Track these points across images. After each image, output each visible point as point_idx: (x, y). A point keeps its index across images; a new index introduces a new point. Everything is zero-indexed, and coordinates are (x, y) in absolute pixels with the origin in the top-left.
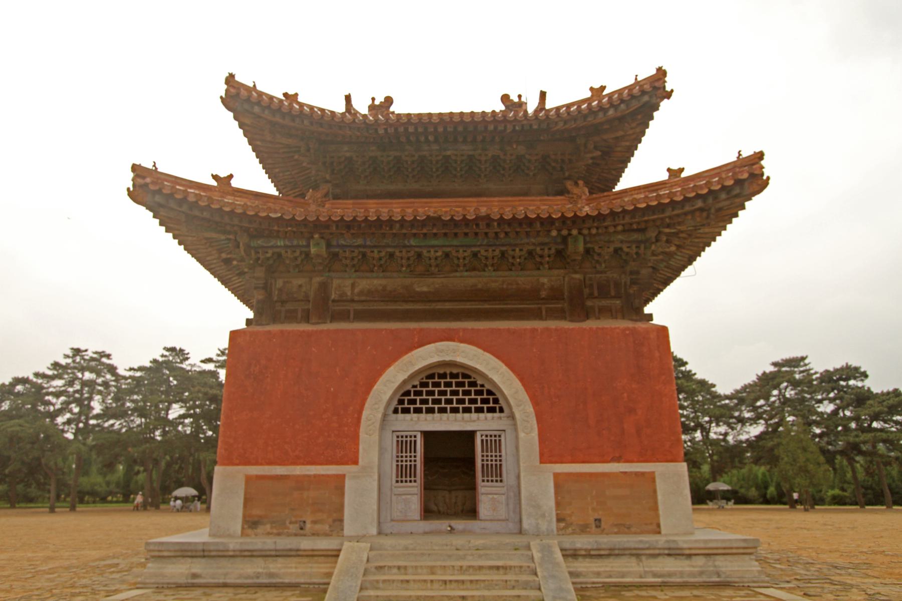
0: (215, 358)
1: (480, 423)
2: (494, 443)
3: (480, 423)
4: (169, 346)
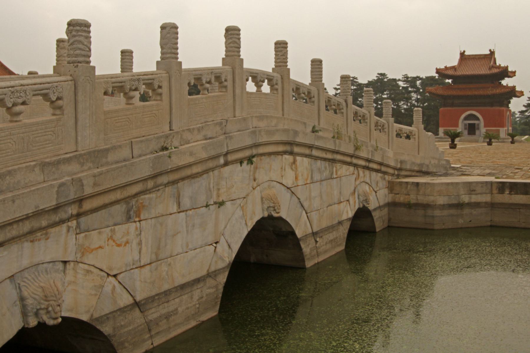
0: (401, 79)
1: (476, 122)
2: (478, 125)
3: (476, 122)
4: (380, 73)
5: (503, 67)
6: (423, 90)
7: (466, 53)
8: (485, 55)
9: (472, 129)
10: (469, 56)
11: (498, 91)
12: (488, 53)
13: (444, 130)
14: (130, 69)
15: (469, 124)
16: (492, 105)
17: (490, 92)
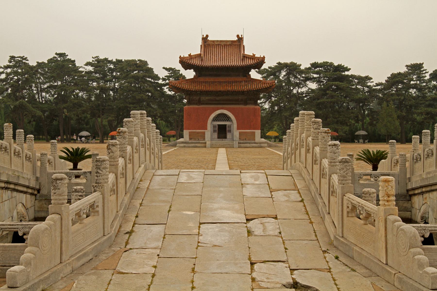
1: (227, 123)
2: (230, 126)
3: (227, 123)
5: (258, 58)
6: (115, 76)
8: (233, 41)
9: (222, 132)
10: (213, 41)
12: (236, 39)
13: (190, 132)
15: (218, 125)
16: (246, 103)
17: (235, 88)
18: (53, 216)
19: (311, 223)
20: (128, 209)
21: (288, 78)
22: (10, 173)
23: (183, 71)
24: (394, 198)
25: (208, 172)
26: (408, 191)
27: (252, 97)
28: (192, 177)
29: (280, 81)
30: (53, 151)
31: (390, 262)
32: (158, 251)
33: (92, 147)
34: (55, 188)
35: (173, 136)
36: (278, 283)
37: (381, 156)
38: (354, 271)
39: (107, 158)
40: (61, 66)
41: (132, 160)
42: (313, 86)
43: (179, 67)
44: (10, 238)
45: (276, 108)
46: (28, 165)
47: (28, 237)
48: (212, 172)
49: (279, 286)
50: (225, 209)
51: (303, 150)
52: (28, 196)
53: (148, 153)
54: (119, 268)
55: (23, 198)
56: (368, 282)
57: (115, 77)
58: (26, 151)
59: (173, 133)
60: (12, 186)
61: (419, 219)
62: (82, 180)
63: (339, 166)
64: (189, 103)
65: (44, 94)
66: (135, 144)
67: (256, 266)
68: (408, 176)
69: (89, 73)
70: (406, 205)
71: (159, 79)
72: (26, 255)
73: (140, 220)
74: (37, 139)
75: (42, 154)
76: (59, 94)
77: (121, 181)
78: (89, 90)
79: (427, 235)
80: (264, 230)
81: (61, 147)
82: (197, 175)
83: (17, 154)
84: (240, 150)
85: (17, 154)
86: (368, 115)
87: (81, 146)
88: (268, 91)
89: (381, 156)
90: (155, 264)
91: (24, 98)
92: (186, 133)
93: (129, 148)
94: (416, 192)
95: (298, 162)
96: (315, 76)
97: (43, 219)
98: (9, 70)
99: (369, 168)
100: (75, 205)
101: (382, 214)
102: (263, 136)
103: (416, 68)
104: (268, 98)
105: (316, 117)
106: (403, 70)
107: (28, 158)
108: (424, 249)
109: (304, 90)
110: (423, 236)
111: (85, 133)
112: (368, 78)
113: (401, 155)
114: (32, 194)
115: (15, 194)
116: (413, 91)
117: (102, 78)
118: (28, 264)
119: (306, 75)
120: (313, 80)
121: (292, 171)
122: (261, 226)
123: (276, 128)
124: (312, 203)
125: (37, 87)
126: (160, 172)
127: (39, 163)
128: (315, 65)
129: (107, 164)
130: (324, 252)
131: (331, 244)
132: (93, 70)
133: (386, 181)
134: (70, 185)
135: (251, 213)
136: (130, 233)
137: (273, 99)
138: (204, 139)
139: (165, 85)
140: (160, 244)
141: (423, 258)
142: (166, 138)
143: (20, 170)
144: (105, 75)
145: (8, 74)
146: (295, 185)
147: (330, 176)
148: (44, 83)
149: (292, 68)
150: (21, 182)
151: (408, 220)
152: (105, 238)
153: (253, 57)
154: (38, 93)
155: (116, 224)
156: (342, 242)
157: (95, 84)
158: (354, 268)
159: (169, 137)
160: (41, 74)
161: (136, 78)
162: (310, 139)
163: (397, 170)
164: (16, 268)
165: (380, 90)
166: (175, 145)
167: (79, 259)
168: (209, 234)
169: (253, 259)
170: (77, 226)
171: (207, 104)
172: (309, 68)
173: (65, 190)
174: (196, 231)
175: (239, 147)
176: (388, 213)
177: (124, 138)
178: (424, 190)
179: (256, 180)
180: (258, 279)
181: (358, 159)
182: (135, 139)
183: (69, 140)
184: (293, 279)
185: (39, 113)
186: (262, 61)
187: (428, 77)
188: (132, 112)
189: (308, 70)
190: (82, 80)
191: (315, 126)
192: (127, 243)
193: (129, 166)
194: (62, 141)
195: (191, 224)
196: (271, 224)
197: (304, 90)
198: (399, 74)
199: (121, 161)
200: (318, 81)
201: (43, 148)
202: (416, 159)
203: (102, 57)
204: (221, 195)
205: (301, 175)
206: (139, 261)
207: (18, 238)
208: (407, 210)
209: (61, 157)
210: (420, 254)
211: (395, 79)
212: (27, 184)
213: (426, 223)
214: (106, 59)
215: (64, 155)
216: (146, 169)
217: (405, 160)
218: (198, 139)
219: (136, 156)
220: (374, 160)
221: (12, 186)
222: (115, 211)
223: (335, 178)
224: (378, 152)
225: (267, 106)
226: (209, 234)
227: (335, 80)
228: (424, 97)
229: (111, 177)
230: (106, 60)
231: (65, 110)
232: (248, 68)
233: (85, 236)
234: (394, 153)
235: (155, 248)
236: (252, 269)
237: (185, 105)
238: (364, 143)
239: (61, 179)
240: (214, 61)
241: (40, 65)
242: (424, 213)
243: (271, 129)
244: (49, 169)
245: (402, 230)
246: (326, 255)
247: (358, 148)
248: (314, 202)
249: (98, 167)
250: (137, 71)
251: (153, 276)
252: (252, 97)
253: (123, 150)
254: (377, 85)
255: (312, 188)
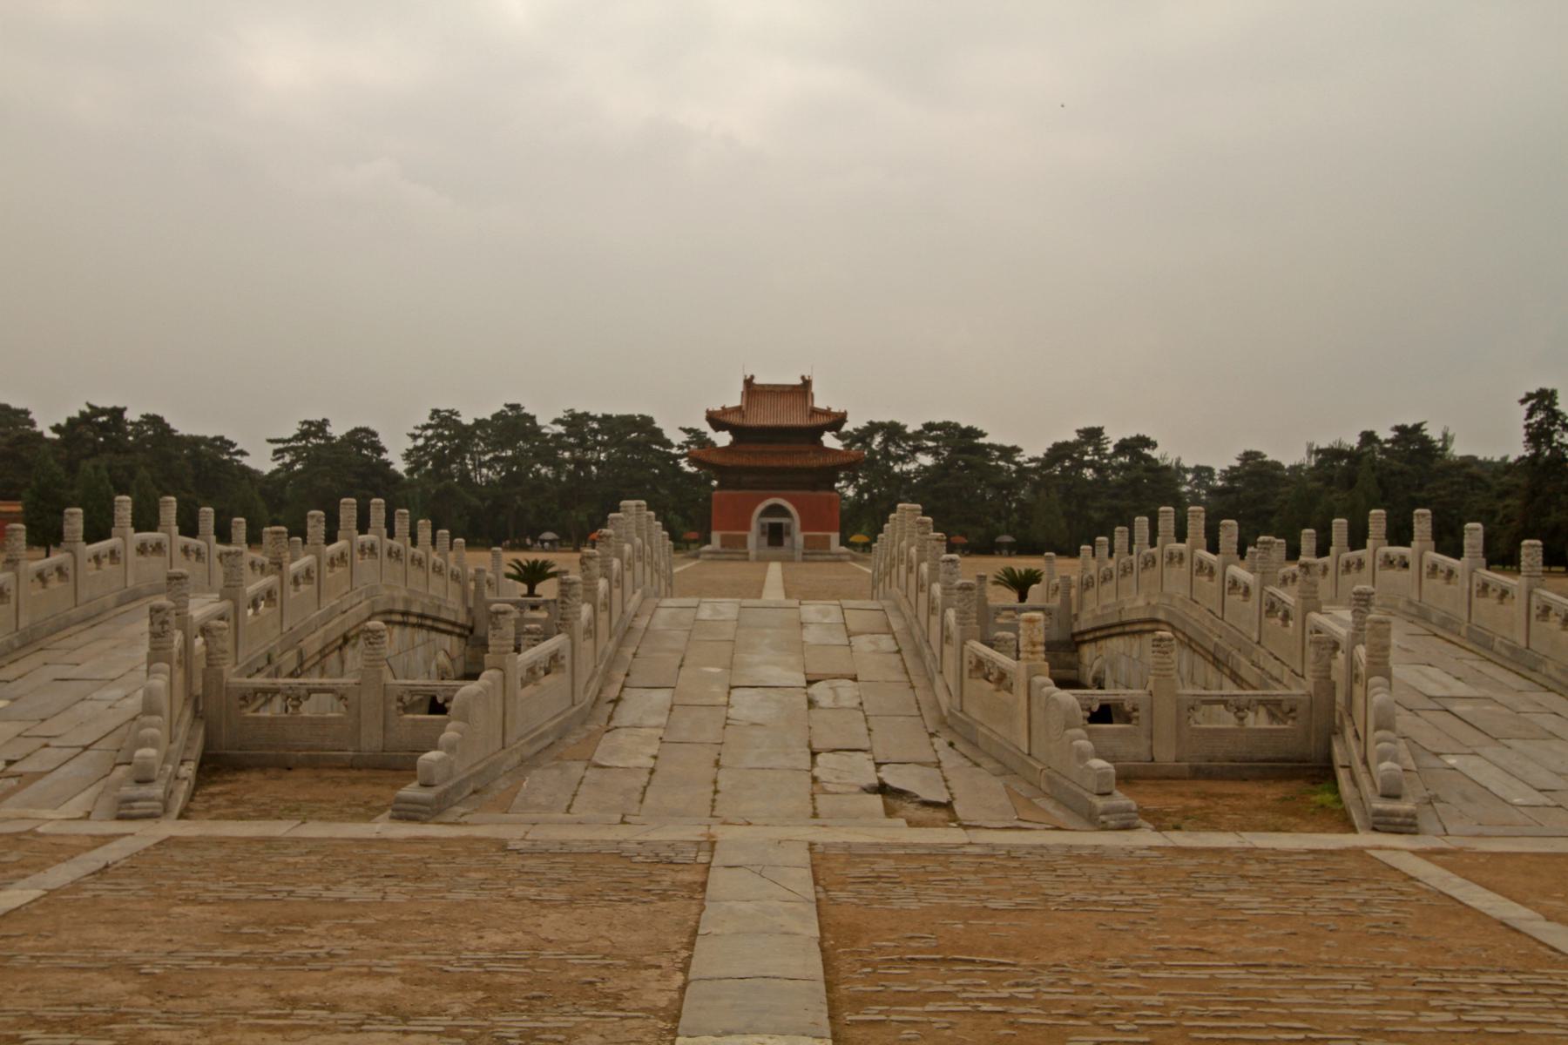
2: (788, 526)
5: (836, 414)
7: (757, 381)
9: (776, 535)
10: (763, 386)
11: (815, 462)
12: (800, 382)
14: (1411, 825)
15: (771, 525)
17: (798, 462)
18: (492, 672)
19: (913, 687)
20: (612, 662)
21: (886, 448)
22: (426, 601)
23: (712, 435)
24: (1042, 648)
25: (747, 602)
26: (1073, 635)
27: (824, 477)
28: (720, 610)
29: (873, 452)
30: (493, 565)
31: (1035, 752)
32: (660, 732)
33: (564, 560)
34: (496, 627)
35: (695, 541)
36: (853, 785)
37: (1032, 578)
38: (977, 765)
39: (578, 578)
40: (512, 425)
41: (620, 582)
42: (927, 460)
43: (705, 427)
44: (425, 706)
45: (866, 496)
46: (454, 587)
47: (452, 706)
48: (755, 602)
49: (856, 789)
50: (775, 664)
51: (903, 568)
52: (455, 639)
53: (648, 569)
54: (596, 759)
55: (448, 642)
56: (998, 783)
57: (600, 443)
58: (452, 565)
59: (693, 535)
60: (429, 622)
61: (1089, 681)
62: (542, 614)
63: (957, 595)
64: (720, 486)
65: (484, 471)
66: (626, 555)
67: (819, 758)
68: (1074, 611)
69: (558, 436)
70: (1070, 658)
71: (671, 445)
72: (450, 734)
73: (635, 679)
74: (471, 544)
75: (478, 571)
76: (509, 471)
77: (603, 616)
78: (558, 464)
79: (1095, 708)
80: (836, 698)
81: (509, 558)
82: (728, 608)
83: (438, 570)
84: (805, 565)
85: (438, 570)
86: (1016, 510)
87: (541, 557)
88: (851, 467)
89: (1032, 578)
90: (655, 752)
91: (453, 477)
92: (716, 537)
93: (616, 563)
94: (1087, 637)
95: (895, 588)
96: (930, 444)
97: (474, 676)
98: (430, 432)
99: (1012, 597)
100: (528, 655)
101: (1023, 674)
102: (844, 542)
103: (1093, 435)
104: (852, 479)
105: (924, 514)
106: (1072, 437)
107: (455, 577)
108: (1089, 732)
109: (912, 466)
110: (1089, 710)
111: (549, 535)
112: (1015, 450)
113: (1063, 578)
114: (460, 636)
115: (433, 635)
116: (1088, 473)
117: (579, 445)
118: (451, 748)
119: (917, 441)
120: (926, 450)
121: (886, 603)
122: (830, 693)
123: (865, 528)
124: (914, 655)
125: (472, 459)
126: (668, 602)
127: (472, 586)
128: (929, 427)
129: (579, 589)
130: (932, 735)
131: (943, 721)
132: (400, 467)
133: (1031, 621)
134: (520, 622)
135: (815, 669)
136: (616, 701)
137: (861, 481)
138: (745, 546)
139: (681, 456)
140: (663, 720)
141: (1086, 744)
142: (680, 543)
143: (442, 596)
144: (583, 440)
145: (428, 439)
146: (888, 625)
147: (944, 611)
148: (485, 453)
149: (893, 431)
150: (444, 615)
151: (1062, 684)
152: (575, 709)
153: (827, 413)
154: (474, 469)
155: (594, 687)
156: (961, 720)
157: (567, 454)
158: (979, 761)
159: (688, 542)
160: (481, 439)
161: (635, 445)
162: (913, 550)
163: (1056, 602)
164: (433, 755)
165: (1035, 470)
166: (696, 557)
167: (532, 742)
168: (745, 705)
169: (816, 746)
170: (530, 689)
171: (752, 488)
172: (920, 432)
173: (509, 629)
174: (723, 700)
175: (804, 560)
176: (1032, 673)
177: (609, 546)
178: (1098, 634)
179: (825, 617)
180: (823, 778)
181: (995, 583)
182: (627, 547)
183: (525, 548)
184: (880, 779)
185: (475, 501)
186: (841, 419)
187: (1110, 450)
188: (623, 503)
189: (918, 435)
190: (547, 448)
191: (922, 529)
192: (610, 718)
193: (617, 592)
194: (512, 548)
195: (716, 689)
196: (847, 691)
197: (912, 466)
198: (1066, 444)
199: (602, 584)
200: (934, 452)
201: (479, 560)
202: (1087, 585)
203: (579, 411)
204: (767, 641)
205: (898, 608)
206: (630, 747)
207: (437, 707)
208: (1071, 666)
209: (508, 576)
210: (1081, 738)
211: (1059, 452)
212: (452, 618)
213: (1101, 687)
214: (586, 414)
215: (513, 571)
216: (644, 597)
217: (1069, 586)
218: (734, 546)
219: (628, 575)
220: (1021, 584)
221: (429, 622)
222: (591, 666)
223: (951, 614)
224: (1028, 572)
225: (850, 492)
226: (745, 705)
227: (962, 451)
228: (1106, 482)
229: (586, 610)
230: (586, 417)
231: (518, 498)
232: (819, 431)
233: (544, 704)
234: (1052, 574)
235: (657, 727)
236: (813, 762)
237: (714, 489)
238: (1010, 555)
239: (505, 613)
240: (763, 417)
241: (480, 424)
242: (1098, 672)
243: (857, 530)
244: (489, 595)
245: (1054, 699)
246: (935, 740)
247: (994, 565)
248: (918, 654)
249: (564, 593)
250: (635, 434)
251: (652, 771)
252: (824, 477)
253: (606, 567)
254: (1031, 461)
255: (916, 630)
